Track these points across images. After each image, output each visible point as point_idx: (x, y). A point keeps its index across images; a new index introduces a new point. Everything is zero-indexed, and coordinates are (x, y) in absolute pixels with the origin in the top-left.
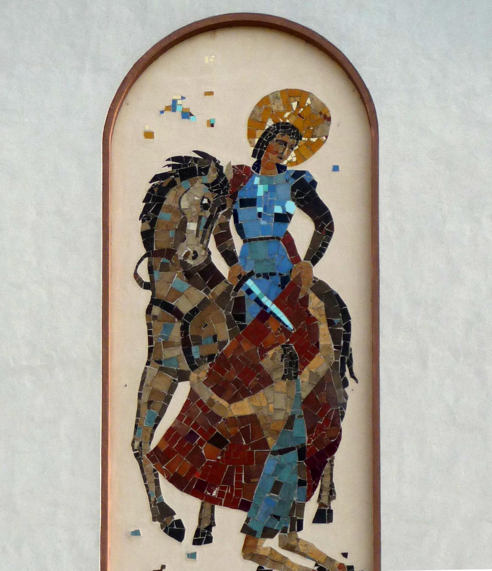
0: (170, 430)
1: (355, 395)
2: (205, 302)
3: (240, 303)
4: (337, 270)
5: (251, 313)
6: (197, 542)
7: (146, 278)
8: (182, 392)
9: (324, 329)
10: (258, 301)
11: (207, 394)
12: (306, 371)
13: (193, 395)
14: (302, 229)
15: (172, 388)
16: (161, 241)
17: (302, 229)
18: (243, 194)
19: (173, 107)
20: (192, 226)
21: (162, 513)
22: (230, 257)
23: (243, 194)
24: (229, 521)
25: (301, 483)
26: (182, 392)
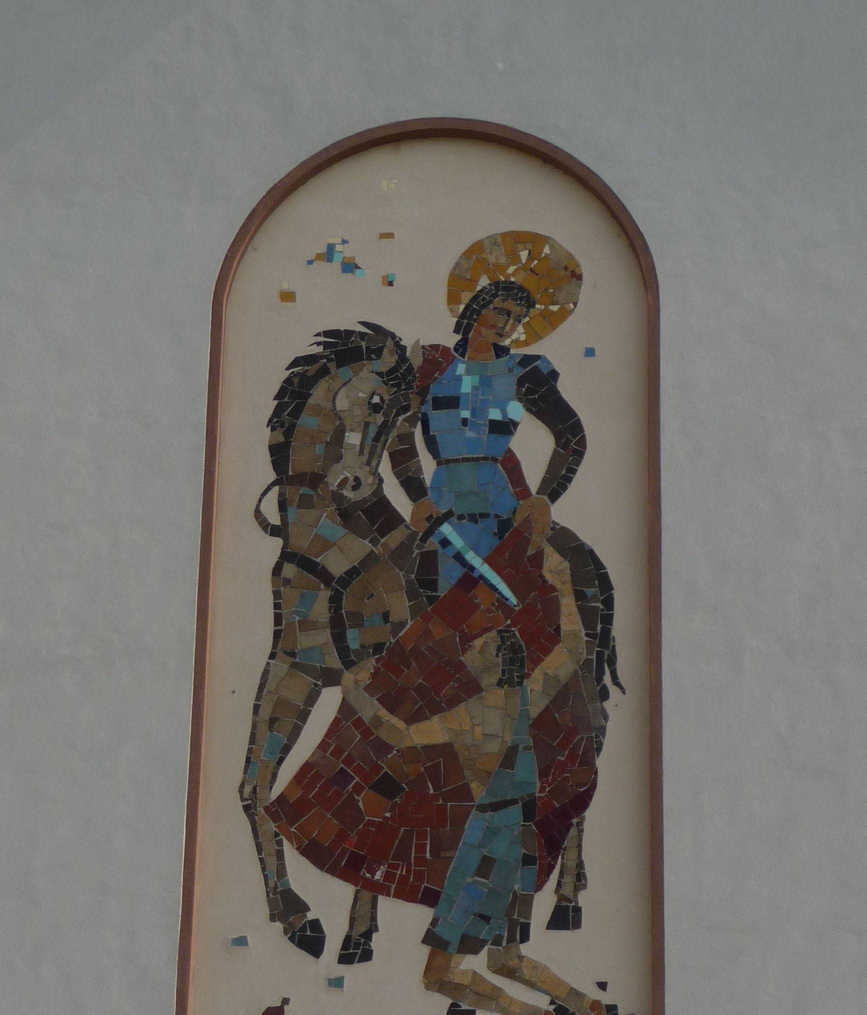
0: (306, 768)
1: (620, 714)
2: (370, 559)
3: (429, 561)
4: (591, 509)
5: (448, 577)
6: (345, 959)
7: (274, 519)
8: (329, 702)
9: (568, 605)
10: (459, 557)
11: (370, 708)
12: (537, 673)
13: (346, 709)
14: (533, 446)
15: (312, 698)
16: (301, 459)
17: (533, 446)
18: (437, 390)
19: (328, 255)
20: (353, 438)
21: (286, 907)
22: (414, 487)
23: (437, 390)
24: (402, 923)
25: (527, 860)
26: (329, 702)
